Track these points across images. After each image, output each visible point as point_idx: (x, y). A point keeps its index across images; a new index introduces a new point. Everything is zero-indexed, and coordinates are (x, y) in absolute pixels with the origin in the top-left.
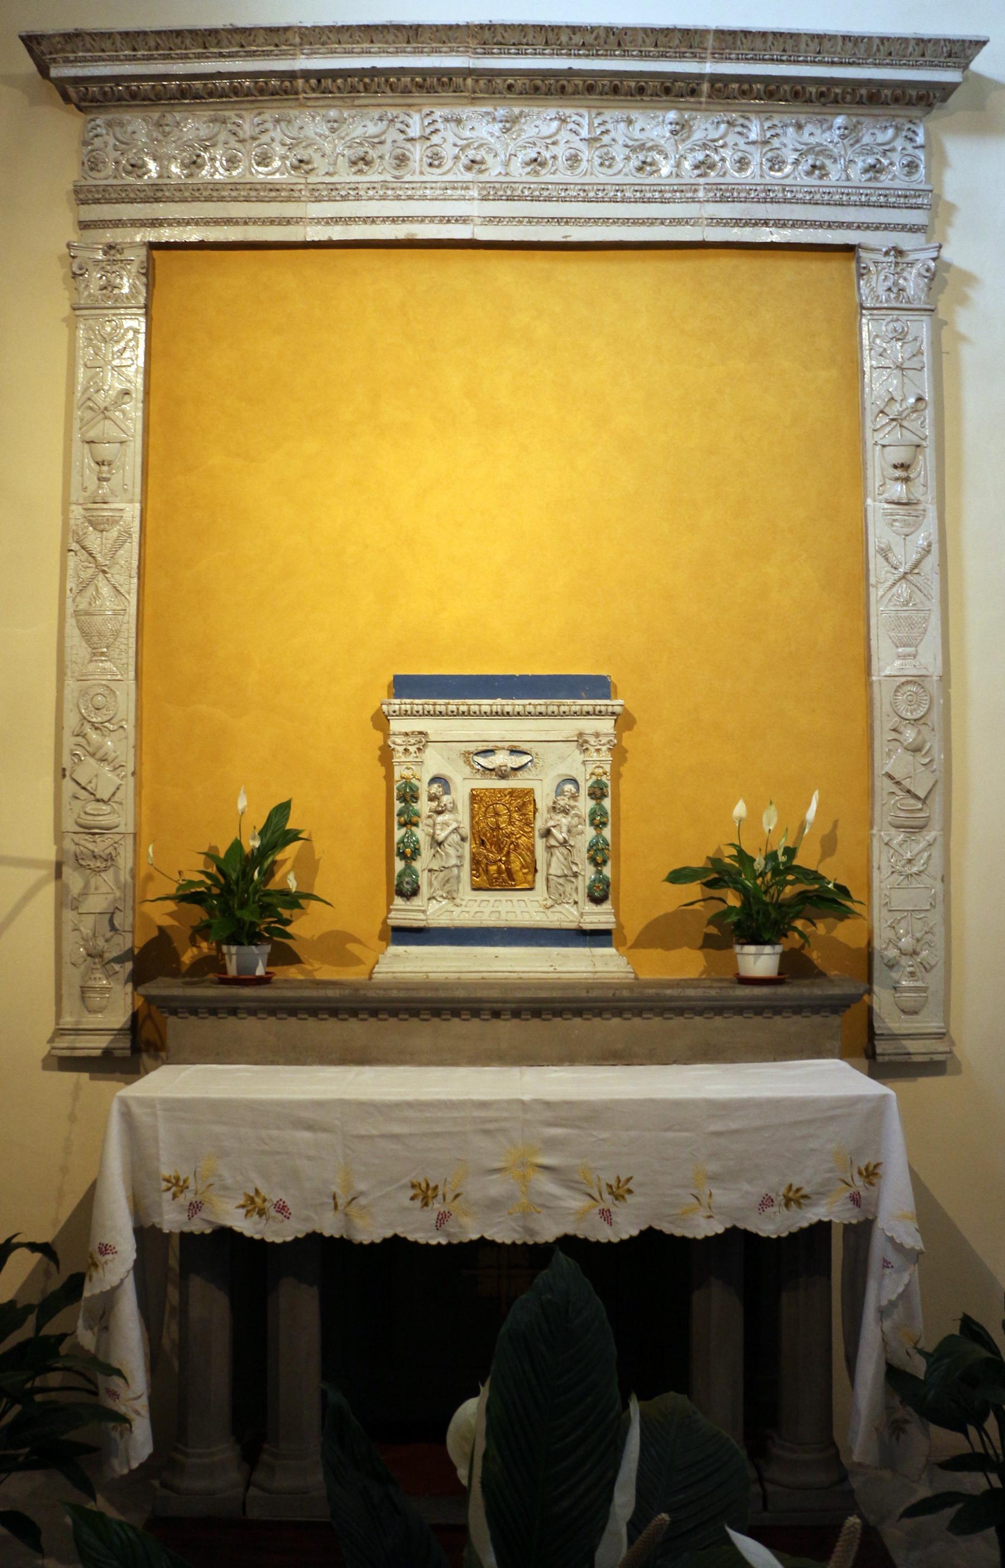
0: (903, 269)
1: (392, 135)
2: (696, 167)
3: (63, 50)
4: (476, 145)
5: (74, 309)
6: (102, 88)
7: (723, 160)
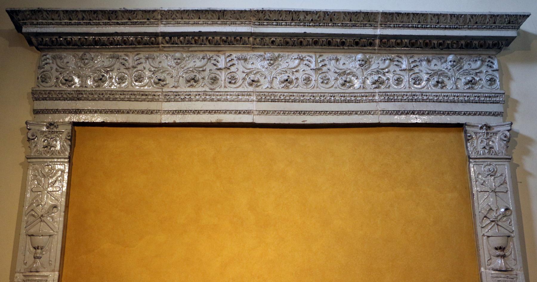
0: (491, 136)
1: (209, 66)
2: (374, 83)
3: (31, 18)
4: (255, 72)
5: (27, 159)
6: (51, 39)
7: (388, 79)
